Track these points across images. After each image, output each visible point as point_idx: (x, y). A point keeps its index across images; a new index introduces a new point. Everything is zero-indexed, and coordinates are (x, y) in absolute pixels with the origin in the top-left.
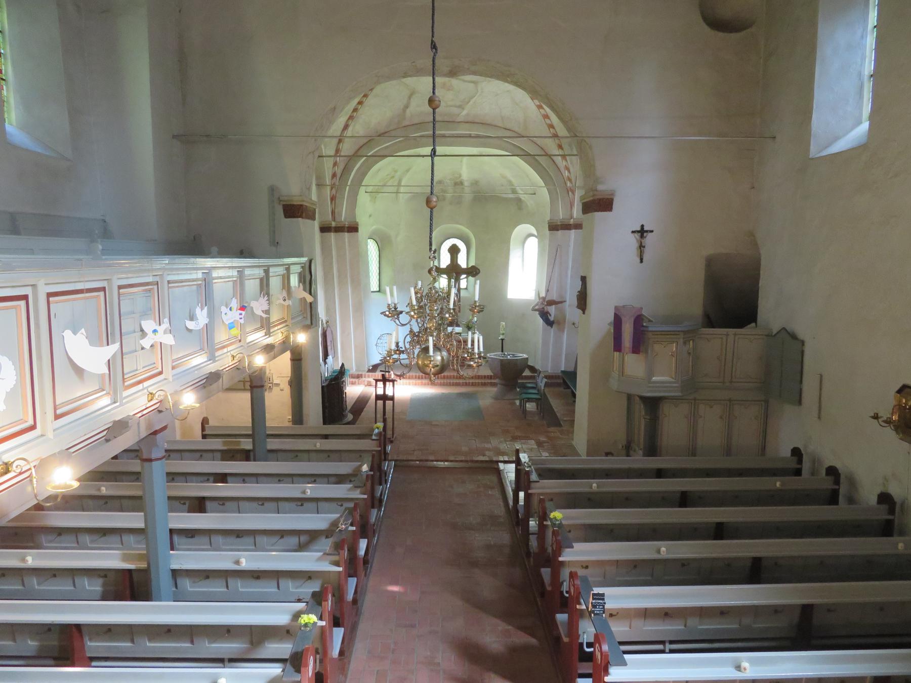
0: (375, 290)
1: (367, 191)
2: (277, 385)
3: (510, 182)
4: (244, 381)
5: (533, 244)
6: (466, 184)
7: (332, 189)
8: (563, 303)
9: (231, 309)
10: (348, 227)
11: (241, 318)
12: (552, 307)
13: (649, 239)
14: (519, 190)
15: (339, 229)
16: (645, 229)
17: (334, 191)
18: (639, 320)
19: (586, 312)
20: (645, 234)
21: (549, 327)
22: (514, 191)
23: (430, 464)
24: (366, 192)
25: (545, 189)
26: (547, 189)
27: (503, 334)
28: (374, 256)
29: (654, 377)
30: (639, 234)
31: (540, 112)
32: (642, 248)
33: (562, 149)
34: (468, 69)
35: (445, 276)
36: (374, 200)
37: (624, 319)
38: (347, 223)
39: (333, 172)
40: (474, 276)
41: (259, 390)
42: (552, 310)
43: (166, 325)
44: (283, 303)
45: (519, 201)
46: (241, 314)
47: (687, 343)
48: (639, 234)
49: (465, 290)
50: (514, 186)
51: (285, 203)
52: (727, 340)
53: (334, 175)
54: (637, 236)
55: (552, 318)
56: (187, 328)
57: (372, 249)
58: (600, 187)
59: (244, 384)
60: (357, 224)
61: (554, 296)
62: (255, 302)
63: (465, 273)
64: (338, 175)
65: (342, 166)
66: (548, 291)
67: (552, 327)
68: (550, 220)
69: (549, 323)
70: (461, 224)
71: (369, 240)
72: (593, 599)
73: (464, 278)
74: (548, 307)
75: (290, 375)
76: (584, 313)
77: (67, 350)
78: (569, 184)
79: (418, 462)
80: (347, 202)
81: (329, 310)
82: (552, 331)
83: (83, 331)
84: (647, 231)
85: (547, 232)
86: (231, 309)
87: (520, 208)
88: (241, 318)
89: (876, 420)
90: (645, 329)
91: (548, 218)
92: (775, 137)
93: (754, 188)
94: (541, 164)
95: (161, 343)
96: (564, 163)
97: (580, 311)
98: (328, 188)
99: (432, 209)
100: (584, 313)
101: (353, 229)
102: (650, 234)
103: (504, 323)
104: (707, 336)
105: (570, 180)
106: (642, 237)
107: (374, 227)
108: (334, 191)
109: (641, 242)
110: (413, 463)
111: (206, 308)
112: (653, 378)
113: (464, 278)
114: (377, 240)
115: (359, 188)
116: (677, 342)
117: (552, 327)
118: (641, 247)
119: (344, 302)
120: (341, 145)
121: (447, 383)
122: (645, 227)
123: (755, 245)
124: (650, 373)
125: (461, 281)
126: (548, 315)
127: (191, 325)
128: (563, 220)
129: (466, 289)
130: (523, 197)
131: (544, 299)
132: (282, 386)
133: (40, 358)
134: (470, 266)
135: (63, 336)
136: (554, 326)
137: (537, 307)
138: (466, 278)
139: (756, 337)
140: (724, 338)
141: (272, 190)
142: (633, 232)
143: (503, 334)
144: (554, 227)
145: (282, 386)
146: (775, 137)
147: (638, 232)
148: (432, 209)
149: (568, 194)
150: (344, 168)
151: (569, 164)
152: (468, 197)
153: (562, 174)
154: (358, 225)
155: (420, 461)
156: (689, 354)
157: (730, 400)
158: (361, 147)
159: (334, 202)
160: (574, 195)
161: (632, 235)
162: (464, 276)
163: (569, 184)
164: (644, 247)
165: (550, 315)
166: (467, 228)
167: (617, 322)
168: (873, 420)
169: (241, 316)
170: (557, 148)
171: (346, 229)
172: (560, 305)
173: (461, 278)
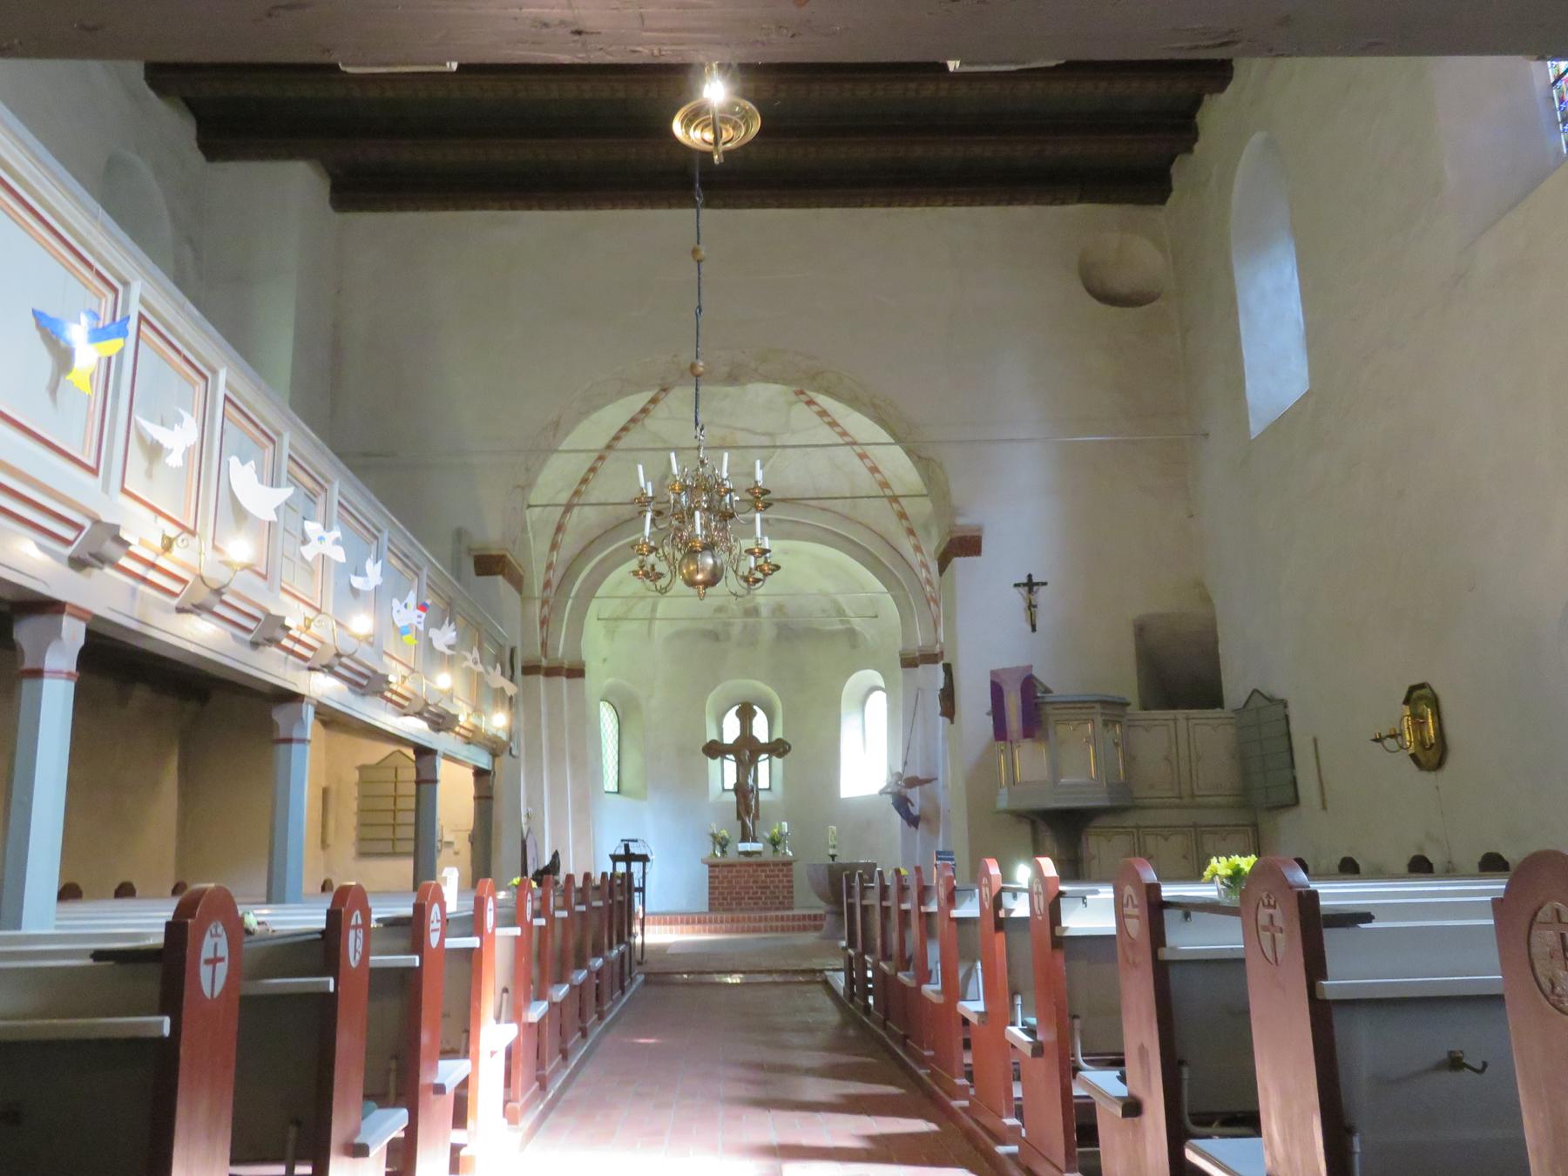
0: (611, 790)
1: (600, 617)
2: (450, 844)
3: (835, 602)
4: (393, 840)
5: (878, 702)
6: (764, 612)
7: (543, 606)
8: (933, 782)
9: (406, 606)
10: (568, 670)
11: (419, 623)
12: (914, 790)
13: (1042, 595)
14: (849, 612)
15: (552, 672)
16: (1035, 580)
17: (546, 610)
18: (1029, 685)
19: (956, 717)
20: (1035, 588)
21: (913, 828)
22: (840, 612)
23: (707, 978)
24: (598, 619)
25: (889, 596)
26: (892, 596)
27: (834, 847)
28: (609, 730)
29: (1062, 778)
30: (1026, 588)
31: (875, 478)
32: (1032, 609)
33: (921, 552)
34: (756, 370)
35: (732, 757)
36: (611, 634)
37: (1006, 688)
38: (566, 662)
39: (549, 561)
40: (780, 755)
41: (429, 785)
42: (915, 794)
43: (336, 533)
44: (473, 666)
45: (851, 634)
46: (420, 617)
47: (1110, 726)
48: (1026, 588)
49: (768, 792)
50: (846, 616)
51: (476, 554)
52: (1176, 728)
53: (547, 584)
54: (1024, 590)
55: (915, 811)
56: (351, 585)
57: (607, 719)
58: (961, 521)
59: (394, 829)
60: (583, 664)
61: (917, 771)
62: (436, 631)
63: (764, 752)
64: (555, 584)
65: (560, 571)
66: (905, 763)
67: (917, 827)
68: (903, 650)
69: (912, 820)
70: (756, 679)
71: (602, 703)
72: (937, 859)
73: (764, 760)
74: (909, 791)
75: (471, 826)
76: (952, 722)
77: (232, 482)
78: (928, 588)
79: (685, 976)
80: (567, 628)
81: (536, 802)
82: (918, 834)
83: (253, 463)
84: (1037, 584)
85: (899, 672)
86: (406, 606)
87: (854, 647)
88: (419, 623)
89: (1379, 744)
90: (1040, 700)
91: (899, 646)
92: (1207, 434)
93: (1192, 516)
94: (882, 563)
95: (323, 556)
96: (919, 557)
97: (947, 720)
98: (538, 604)
99: (699, 262)
100: (952, 722)
101: (577, 672)
102: (1043, 589)
103: (834, 828)
104: (1142, 723)
105: (929, 582)
106: (1030, 591)
107: (610, 680)
108: (546, 610)
109: (1030, 601)
110: (678, 976)
111: (380, 562)
112: (1062, 780)
113: (764, 760)
114: (616, 705)
115: (590, 601)
116: (1093, 720)
117: (917, 827)
118: (1031, 606)
119: (558, 790)
120: (560, 536)
121: (738, 918)
122: (1033, 578)
123: (1207, 599)
124: (1056, 770)
125: (759, 764)
126: (909, 804)
127: (357, 582)
128: (923, 648)
129: (770, 789)
130: (857, 624)
131: (900, 776)
132: (456, 847)
133: (210, 458)
134: (774, 739)
135: (229, 463)
136: (920, 825)
137: (889, 790)
138: (768, 758)
139: (1220, 721)
140: (1171, 724)
141: (459, 534)
142: (1016, 585)
143: (834, 847)
144: (909, 662)
145: (456, 847)
146: (1207, 434)
147: (1024, 585)
148: (699, 262)
149: (929, 604)
150: (564, 575)
151: (928, 559)
152: (767, 631)
153: (916, 575)
154: (584, 665)
155: (688, 973)
156: (1116, 745)
157: (1195, 826)
158: (593, 541)
159: (545, 626)
160: (938, 606)
161: (1015, 590)
162: (764, 756)
163: (928, 588)
164: (1035, 606)
165: (913, 805)
166: (769, 685)
167: (997, 692)
168: (1375, 743)
169: (419, 620)
170: (905, 534)
171: (564, 672)
172: (927, 786)
173: (760, 759)
